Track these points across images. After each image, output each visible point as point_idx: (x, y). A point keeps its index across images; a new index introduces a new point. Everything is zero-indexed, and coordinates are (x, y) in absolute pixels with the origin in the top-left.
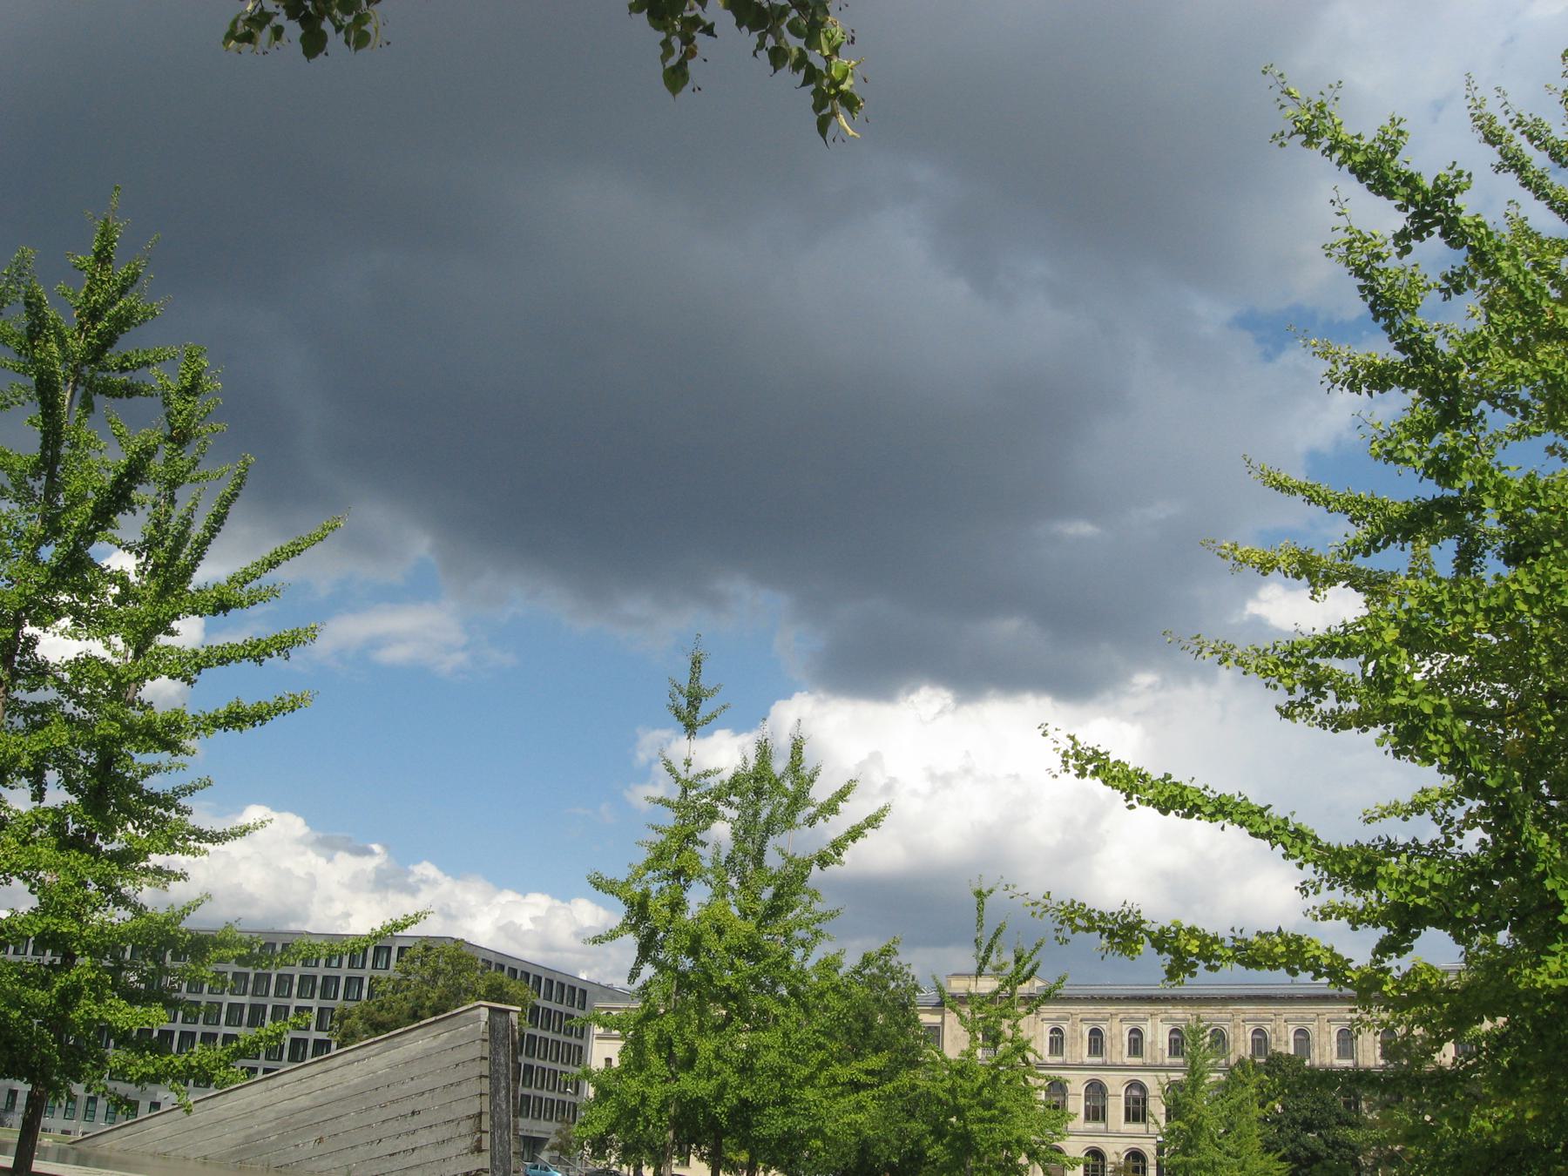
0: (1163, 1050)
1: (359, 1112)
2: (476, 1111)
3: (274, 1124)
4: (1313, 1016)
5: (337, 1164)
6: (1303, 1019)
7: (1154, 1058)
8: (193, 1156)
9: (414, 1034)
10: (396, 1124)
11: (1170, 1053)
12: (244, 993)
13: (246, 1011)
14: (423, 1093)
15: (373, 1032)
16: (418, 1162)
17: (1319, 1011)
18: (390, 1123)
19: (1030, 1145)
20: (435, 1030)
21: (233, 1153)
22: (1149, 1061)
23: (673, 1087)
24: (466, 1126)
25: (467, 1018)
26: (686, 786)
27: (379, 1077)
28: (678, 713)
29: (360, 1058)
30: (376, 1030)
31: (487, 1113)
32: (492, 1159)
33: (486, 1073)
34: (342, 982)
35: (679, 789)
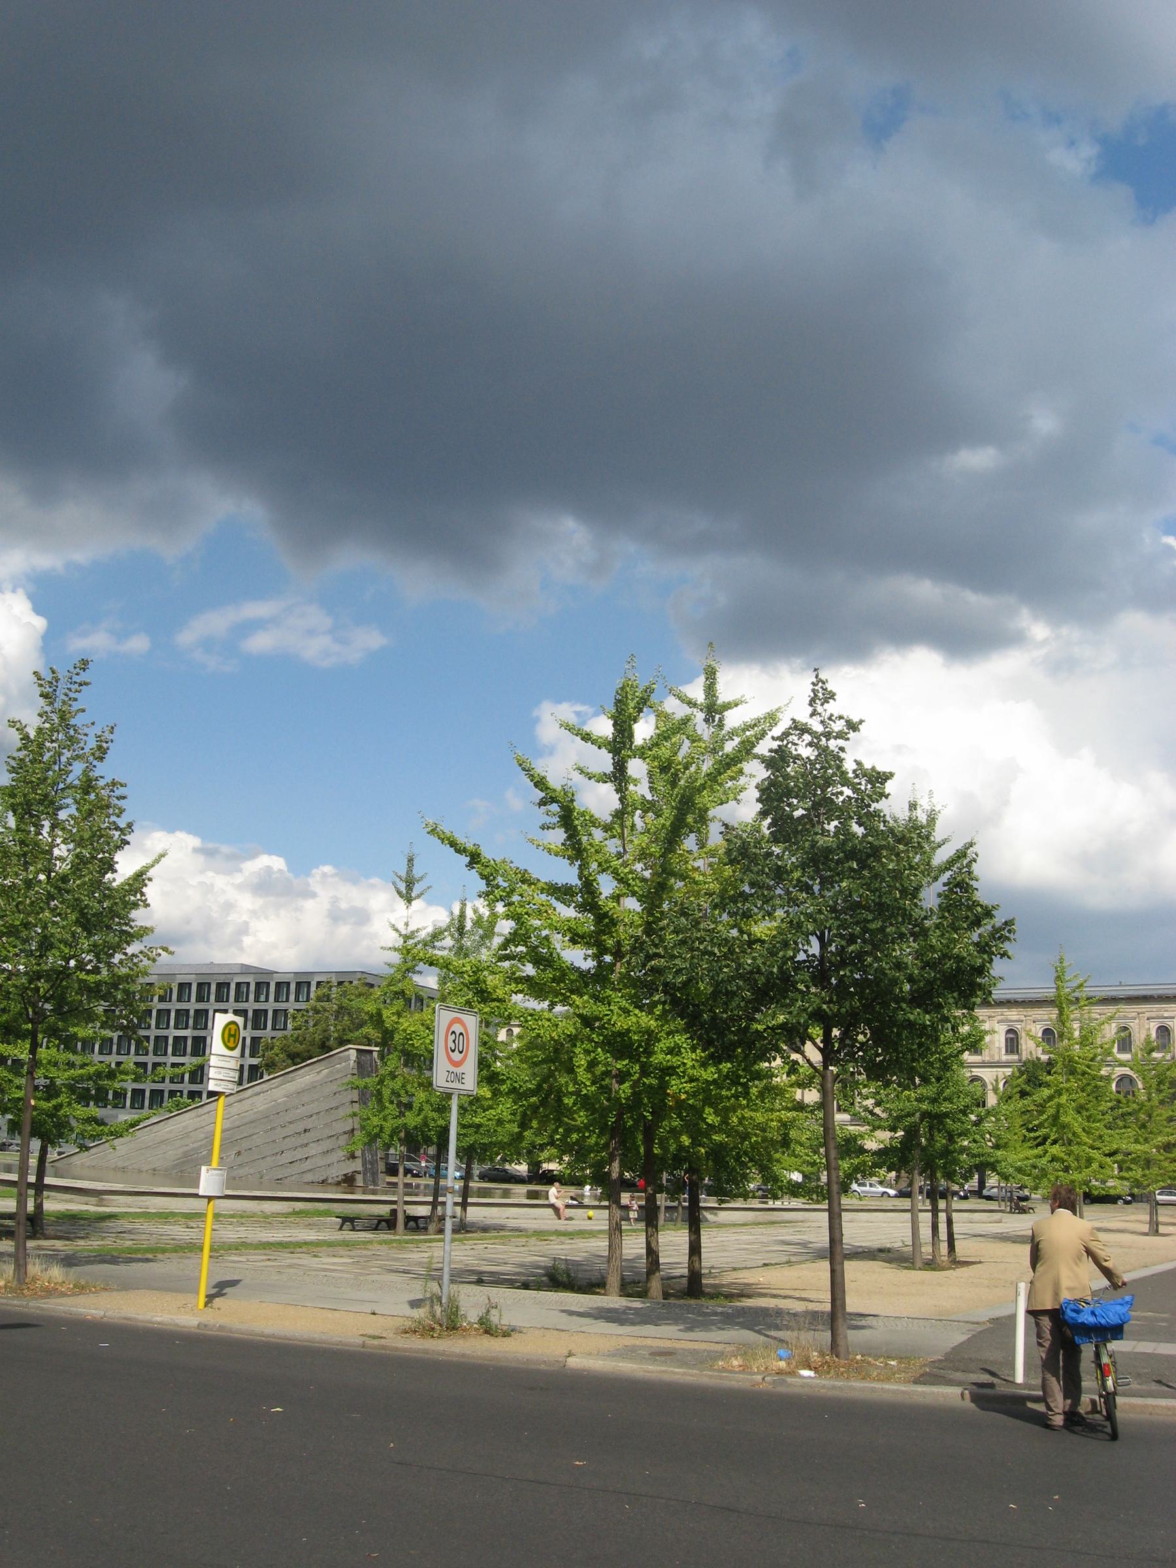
0: (1000, 1049)
1: (266, 1132)
2: (349, 1128)
3: (204, 1142)
4: (1134, 1014)
5: (252, 1171)
6: (1125, 1018)
7: (992, 1056)
9: (302, 1071)
10: (294, 1139)
11: (1007, 1051)
12: (186, 1028)
13: (189, 1042)
14: (311, 1116)
15: (290, 1061)
16: (310, 1167)
17: (1140, 1010)
18: (288, 1139)
20: (318, 1067)
21: (176, 1165)
22: (987, 1059)
23: (400, 1121)
25: (340, 1058)
26: (406, 938)
27: (279, 1104)
28: (399, 893)
30: (292, 1059)
32: (364, 1164)
34: (270, 1014)
35: (401, 940)
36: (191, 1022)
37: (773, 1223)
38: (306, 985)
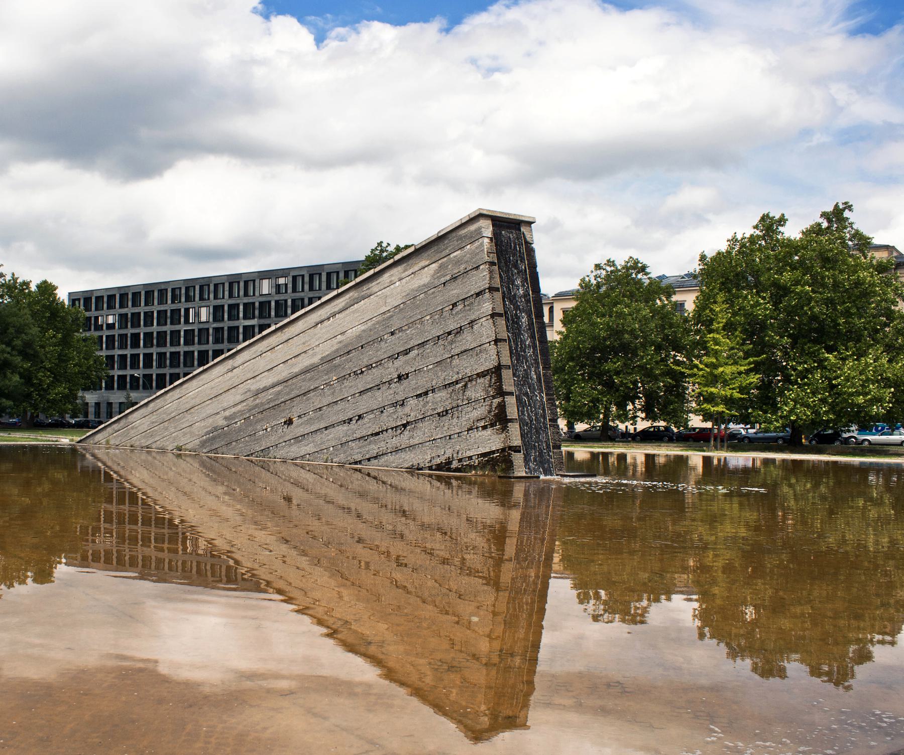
8: (170, 448)
9: (386, 277)
12: (254, 318)
19: (695, 554)
24: (477, 391)
25: (461, 238)
29: (323, 318)
31: (508, 367)
33: (500, 310)
36: (257, 312)
37: (270, 600)
38: (192, 288)
